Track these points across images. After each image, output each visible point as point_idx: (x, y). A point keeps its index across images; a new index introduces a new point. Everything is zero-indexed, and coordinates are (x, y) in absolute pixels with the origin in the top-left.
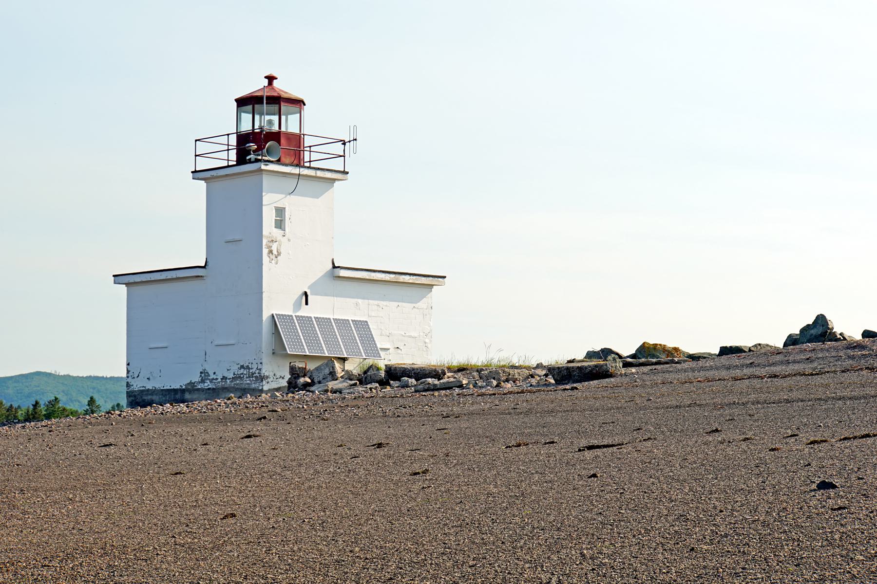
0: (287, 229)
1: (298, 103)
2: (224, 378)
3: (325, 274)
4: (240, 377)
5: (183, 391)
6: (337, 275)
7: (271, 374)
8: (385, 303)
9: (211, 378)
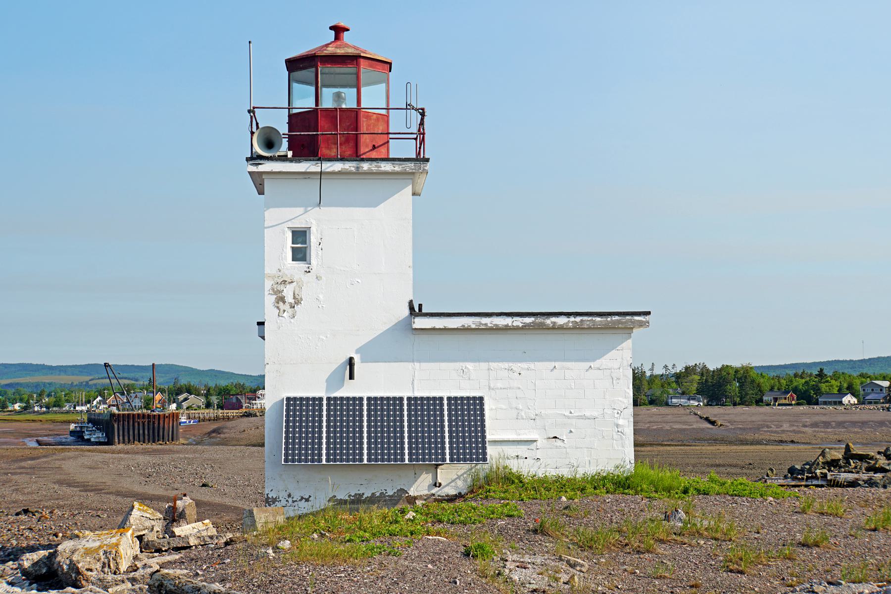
0: (314, 261)
3: (396, 324)
6: (415, 326)
7: (283, 495)
8: (525, 365)
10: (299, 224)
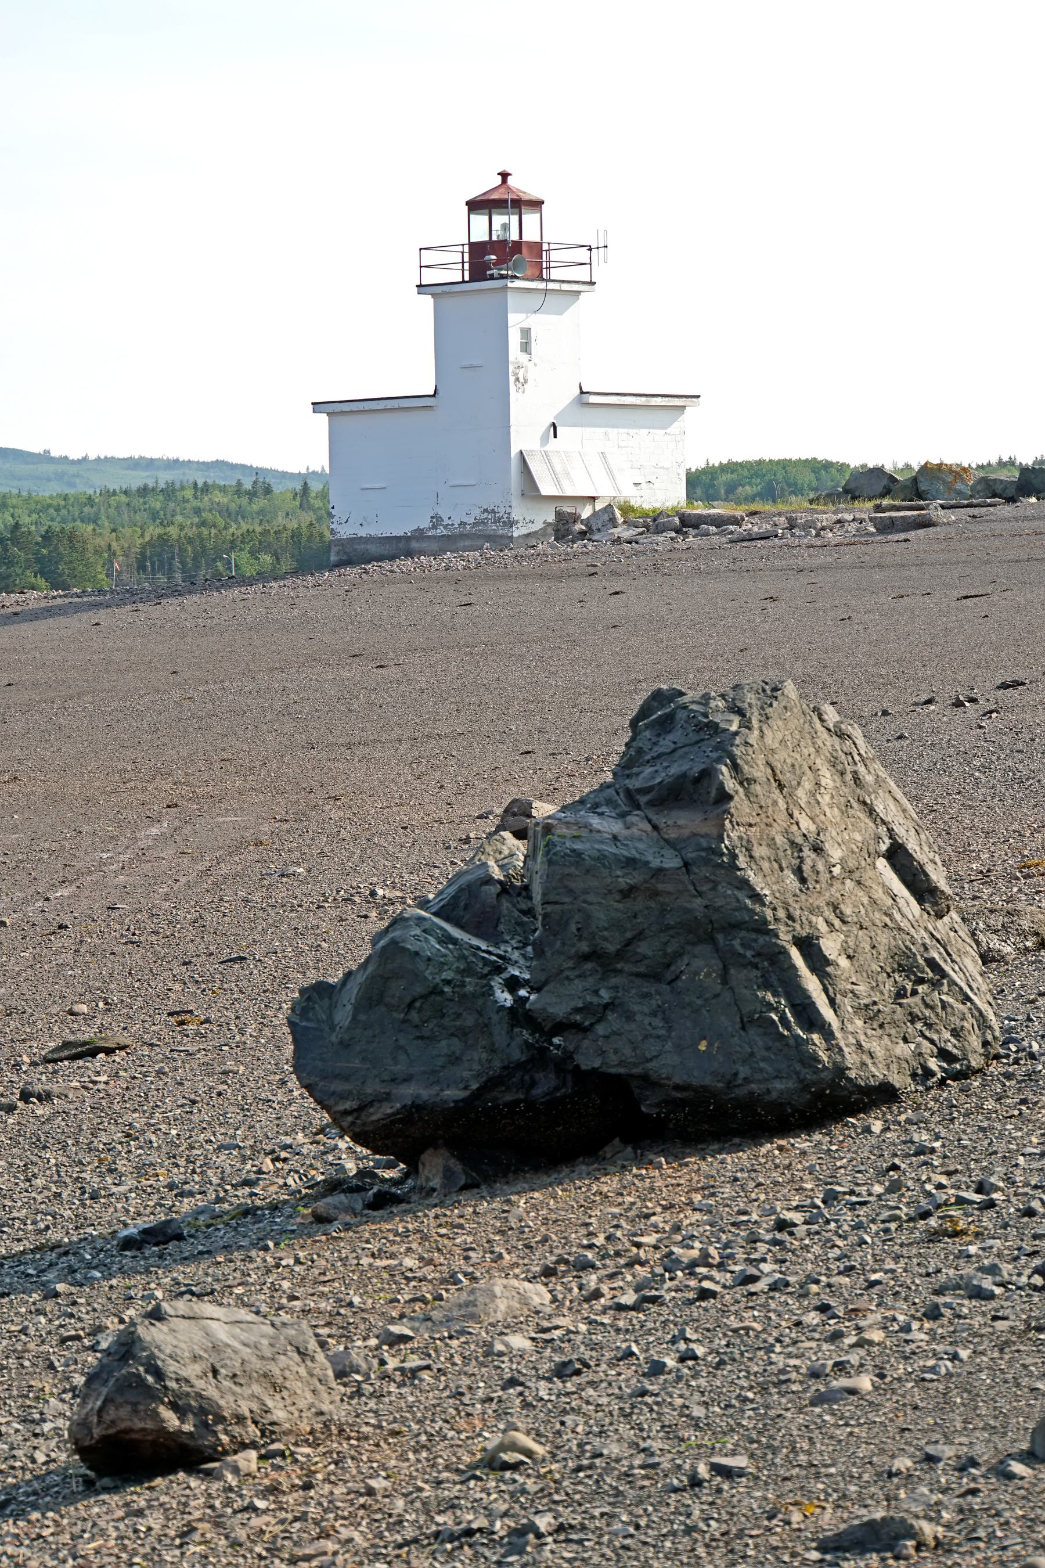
1: (537, 205)
2: (462, 524)
4: (483, 522)
5: (406, 539)
6: (585, 401)
7: (521, 518)
8: (635, 431)
9: (445, 523)
10: (525, 325)
